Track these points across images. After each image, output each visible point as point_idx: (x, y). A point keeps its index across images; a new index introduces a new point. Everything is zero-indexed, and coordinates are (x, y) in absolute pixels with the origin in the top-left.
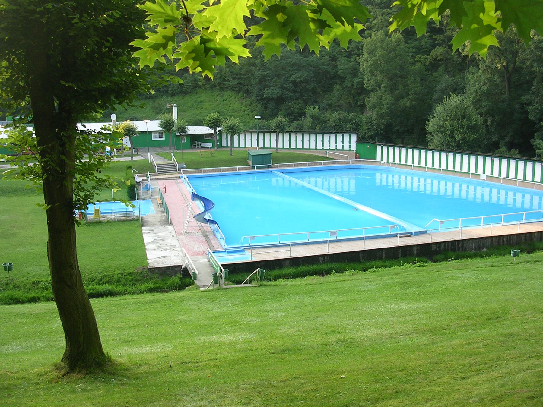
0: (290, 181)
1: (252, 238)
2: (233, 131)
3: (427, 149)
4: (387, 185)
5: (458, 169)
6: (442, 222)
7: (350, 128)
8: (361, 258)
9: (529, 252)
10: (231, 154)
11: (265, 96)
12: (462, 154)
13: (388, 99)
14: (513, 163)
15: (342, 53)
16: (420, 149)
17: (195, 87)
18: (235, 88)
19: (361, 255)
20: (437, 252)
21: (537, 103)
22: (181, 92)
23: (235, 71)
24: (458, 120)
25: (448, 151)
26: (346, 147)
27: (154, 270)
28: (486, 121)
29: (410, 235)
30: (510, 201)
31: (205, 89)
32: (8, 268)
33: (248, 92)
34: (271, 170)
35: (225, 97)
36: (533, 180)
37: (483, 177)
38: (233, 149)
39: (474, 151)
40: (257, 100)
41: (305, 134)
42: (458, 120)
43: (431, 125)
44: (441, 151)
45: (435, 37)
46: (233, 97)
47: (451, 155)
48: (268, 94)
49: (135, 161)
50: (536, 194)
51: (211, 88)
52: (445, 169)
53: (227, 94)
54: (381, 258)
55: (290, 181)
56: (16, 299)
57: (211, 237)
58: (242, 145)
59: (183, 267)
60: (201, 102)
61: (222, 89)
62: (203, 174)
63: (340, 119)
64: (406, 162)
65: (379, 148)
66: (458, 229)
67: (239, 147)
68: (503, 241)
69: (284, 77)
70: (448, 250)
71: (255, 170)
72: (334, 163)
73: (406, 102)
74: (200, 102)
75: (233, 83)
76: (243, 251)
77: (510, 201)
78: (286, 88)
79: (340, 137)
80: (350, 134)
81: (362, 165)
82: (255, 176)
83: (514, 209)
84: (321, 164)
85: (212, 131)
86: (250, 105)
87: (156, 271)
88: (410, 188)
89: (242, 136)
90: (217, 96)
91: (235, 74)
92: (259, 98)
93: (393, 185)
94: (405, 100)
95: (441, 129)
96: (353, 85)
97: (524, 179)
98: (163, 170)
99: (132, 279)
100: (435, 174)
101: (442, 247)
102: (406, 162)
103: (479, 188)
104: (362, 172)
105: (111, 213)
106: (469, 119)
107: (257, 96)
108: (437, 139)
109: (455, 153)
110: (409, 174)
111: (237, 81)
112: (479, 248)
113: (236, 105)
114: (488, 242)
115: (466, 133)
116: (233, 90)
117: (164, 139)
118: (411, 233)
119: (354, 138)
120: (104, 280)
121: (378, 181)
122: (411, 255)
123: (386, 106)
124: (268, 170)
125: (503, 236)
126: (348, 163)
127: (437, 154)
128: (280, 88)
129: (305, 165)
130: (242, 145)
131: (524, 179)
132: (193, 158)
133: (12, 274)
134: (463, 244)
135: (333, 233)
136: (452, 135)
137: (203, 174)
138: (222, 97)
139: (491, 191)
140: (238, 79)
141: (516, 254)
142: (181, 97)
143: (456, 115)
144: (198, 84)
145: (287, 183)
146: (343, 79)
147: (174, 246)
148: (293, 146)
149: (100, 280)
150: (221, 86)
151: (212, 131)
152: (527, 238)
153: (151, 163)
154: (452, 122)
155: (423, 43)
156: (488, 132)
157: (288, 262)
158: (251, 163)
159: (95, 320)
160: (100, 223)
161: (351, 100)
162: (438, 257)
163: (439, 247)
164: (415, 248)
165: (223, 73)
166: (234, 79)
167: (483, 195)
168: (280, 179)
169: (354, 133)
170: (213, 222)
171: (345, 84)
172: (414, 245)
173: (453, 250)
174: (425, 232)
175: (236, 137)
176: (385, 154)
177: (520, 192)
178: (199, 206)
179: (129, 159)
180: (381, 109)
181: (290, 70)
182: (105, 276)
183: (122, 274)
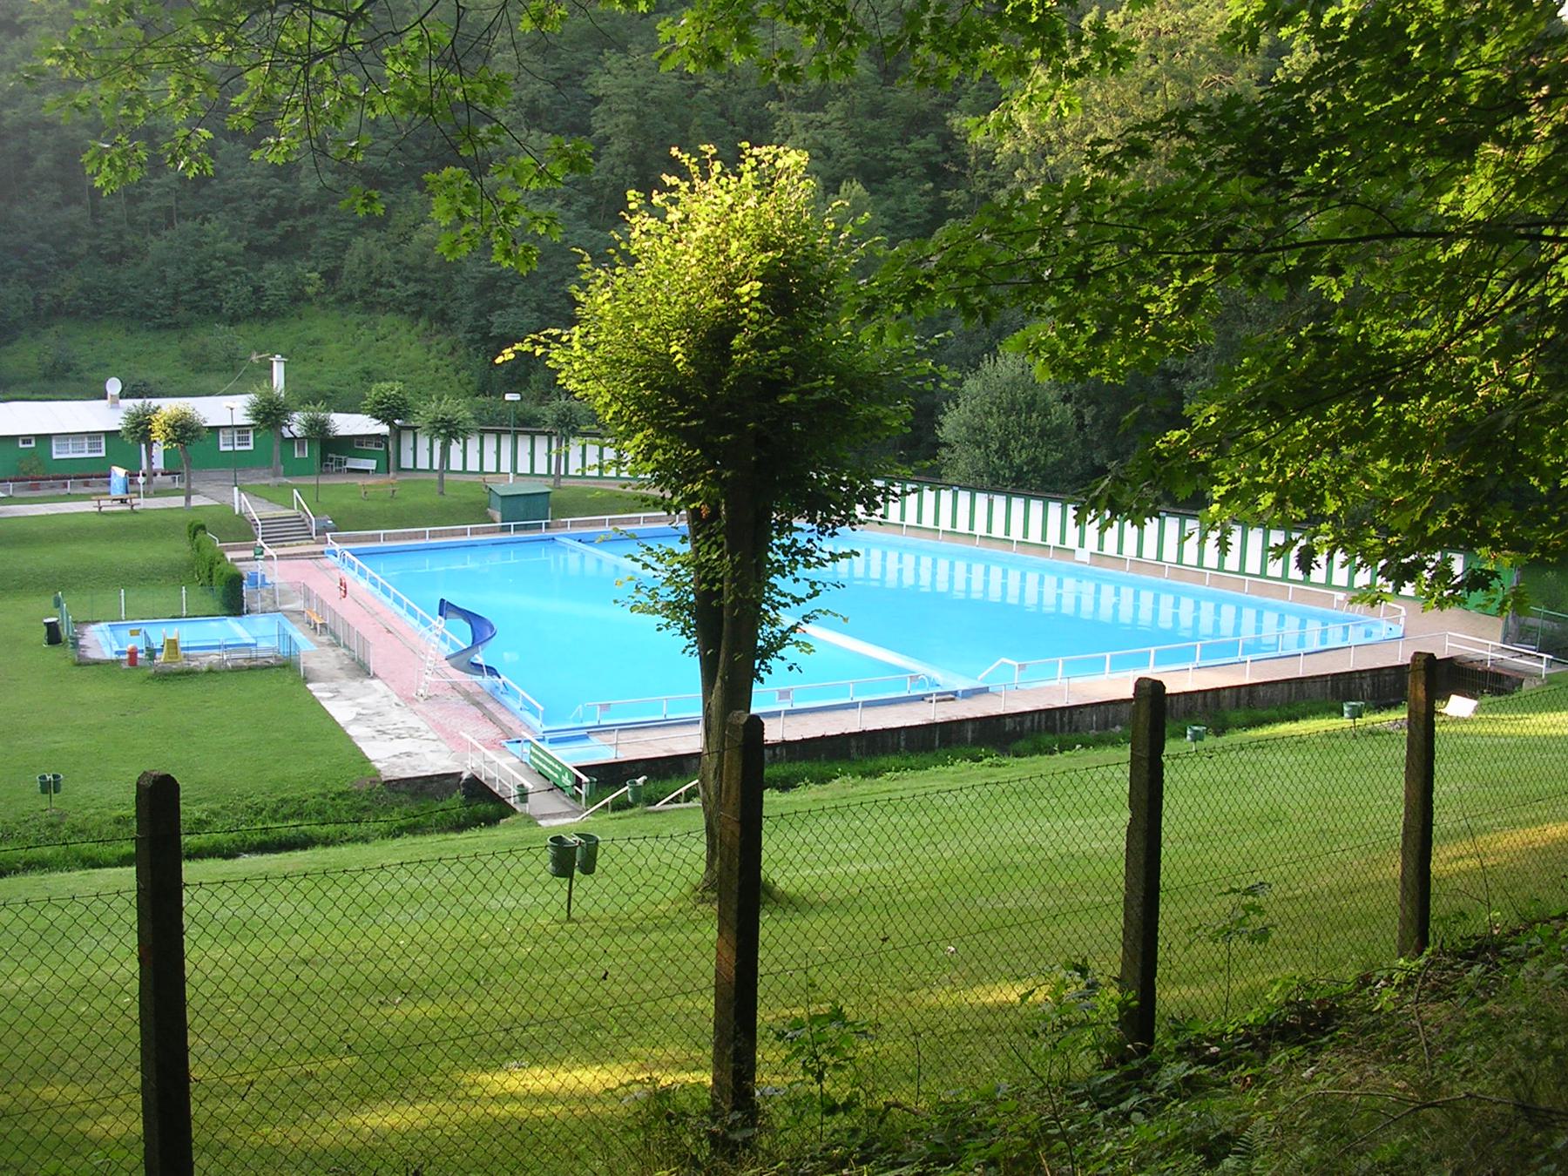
1: (605, 707)
2: (449, 430)
3: (937, 487)
4: (917, 586)
5: (1016, 534)
6: (1022, 667)
8: (853, 751)
9: (1218, 734)
10: (442, 493)
11: (494, 332)
12: (1028, 497)
17: (295, 300)
18: (408, 305)
19: (853, 743)
20: (1017, 735)
21: (1204, 374)
23: (408, 261)
24: (1019, 414)
25: (993, 490)
27: (395, 785)
28: (1079, 415)
29: (952, 696)
30: (1145, 615)
31: (324, 305)
32: (50, 787)
33: (443, 318)
34: (550, 534)
35: (382, 331)
36: (1200, 565)
37: (1083, 555)
38: (446, 477)
39: (1056, 492)
40: (471, 341)
42: (1019, 414)
43: (951, 425)
44: (974, 490)
45: (945, 194)
46: (403, 329)
47: (1000, 501)
48: (504, 325)
50: (1209, 597)
51: (340, 301)
52: (985, 534)
53: (386, 321)
54: (895, 750)
55: (599, 561)
56: (91, 859)
57: (491, 706)
58: (473, 465)
59: (465, 776)
60: (315, 342)
61: (369, 307)
62: (382, 544)
64: (919, 521)
66: (1056, 683)
67: (464, 471)
69: (544, 282)
70: (1039, 731)
71: (512, 535)
74: (313, 343)
75: (404, 290)
76: (586, 737)
77: (1145, 615)
78: (551, 311)
82: (512, 549)
83: (1171, 635)
85: (384, 429)
86: (451, 354)
87: (403, 787)
89: (473, 444)
90: (358, 325)
91: (406, 267)
92: (477, 336)
93: (882, 580)
95: (978, 436)
97: (1179, 562)
98: (280, 532)
99: (351, 808)
100: (961, 546)
101: (1028, 724)
102: (919, 521)
103: (1069, 583)
105: (219, 647)
106: (1045, 413)
107: (472, 330)
108: (964, 460)
109: (1009, 495)
110: (891, 545)
111: (412, 288)
112: (1106, 725)
113: (415, 353)
115: (1037, 446)
116: (402, 311)
117: (251, 447)
118: (955, 693)
120: (286, 810)
122: (962, 741)
124: (544, 533)
127: (964, 496)
128: (533, 310)
130: (473, 465)
131: (1179, 562)
132: (346, 501)
134: (1071, 715)
136: (1003, 451)
137: (382, 544)
138: (373, 328)
139: (1098, 590)
140: (416, 281)
141: (1197, 737)
142: (257, 327)
143: (1013, 403)
144: (302, 292)
147: (418, 730)
149: (275, 811)
150: (370, 298)
151: (384, 429)
152: (1209, 700)
153: (241, 515)
154: (1003, 418)
155: (908, 204)
156: (1085, 442)
158: (498, 516)
160: (190, 673)
162: (1020, 745)
163: (1021, 724)
164: (970, 727)
165: (375, 264)
166: (407, 280)
167: (1078, 600)
168: (573, 559)
172: (968, 720)
173: (1052, 730)
174: (985, 691)
175: (455, 448)
177: (1170, 592)
178: (461, 633)
179: (179, 501)
181: (561, 265)
182: (284, 801)
183: (324, 796)
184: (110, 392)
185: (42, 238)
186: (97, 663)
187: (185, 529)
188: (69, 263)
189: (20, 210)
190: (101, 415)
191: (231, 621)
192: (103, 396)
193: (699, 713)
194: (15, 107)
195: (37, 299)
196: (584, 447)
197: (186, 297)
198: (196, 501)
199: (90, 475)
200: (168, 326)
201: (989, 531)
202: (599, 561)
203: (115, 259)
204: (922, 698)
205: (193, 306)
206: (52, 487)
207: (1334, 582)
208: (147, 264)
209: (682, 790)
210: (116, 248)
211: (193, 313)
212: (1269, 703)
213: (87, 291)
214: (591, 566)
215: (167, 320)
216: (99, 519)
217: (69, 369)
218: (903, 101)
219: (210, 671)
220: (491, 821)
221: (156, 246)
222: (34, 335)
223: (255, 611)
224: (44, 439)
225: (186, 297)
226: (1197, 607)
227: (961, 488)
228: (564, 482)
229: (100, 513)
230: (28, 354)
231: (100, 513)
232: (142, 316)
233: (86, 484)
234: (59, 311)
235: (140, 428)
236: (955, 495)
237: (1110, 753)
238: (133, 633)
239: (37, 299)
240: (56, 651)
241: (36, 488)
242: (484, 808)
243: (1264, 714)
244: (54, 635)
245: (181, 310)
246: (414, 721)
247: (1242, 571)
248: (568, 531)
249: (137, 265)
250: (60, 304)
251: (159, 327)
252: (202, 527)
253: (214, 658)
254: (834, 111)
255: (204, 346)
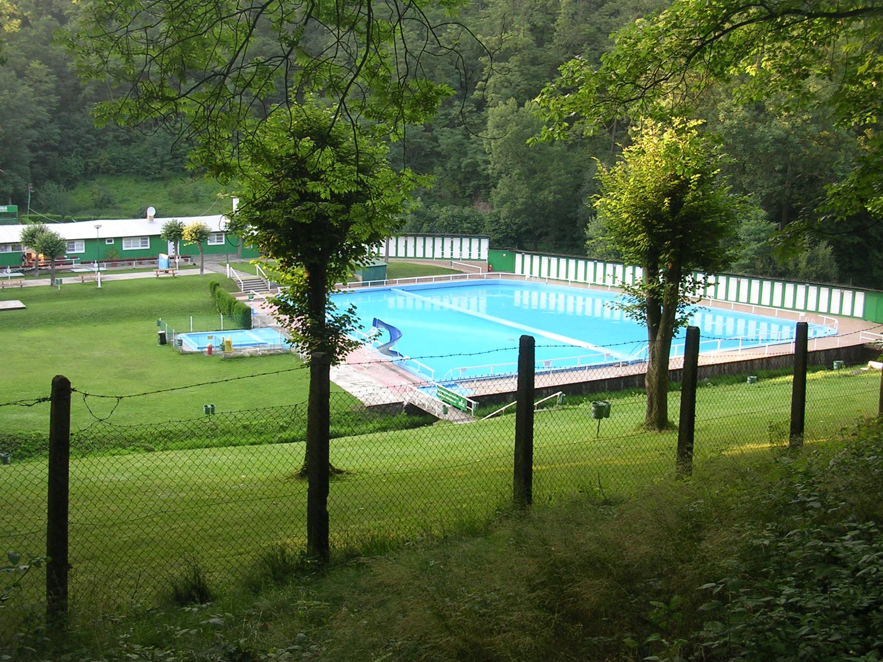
0: (451, 303)
1: (464, 370)
3: (586, 259)
7: (468, 228)
13: (523, 192)
14: (545, 259)
15: (439, 120)
16: (577, 259)
19: (584, 387)
27: (371, 408)
29: (625, 364)
32: (210, 411)
34: (388, 287)
36: (748, 302)
41: (427, 239)
49: (206, 275)
50: (731, 315)
59: (405, 403)
63: (453, 216)
65: (518, 257)
71: (369, 288)
72: (465, 277)
73: (547, 195)
79: (457, 242)
81: (500, 279)
82: (369, 296)
84: (448, 278)
88: (545, 307)
94: (546, 192)
96: (459, 167)
97: (737, 301)
104: (501, 288)
119: (485, 243)
121: (517, 302)
122: (633, 386)
123: (521, 200)
124: (385, 287)
125: (725, 363)
126: (480, 277)
127: (600, 265)
131: (737, 301)
133: (214, 419)
145: (419, 305)
146: (447, 157)
148: (410, 254)
153: (231, 279)
157: (511, 396)
158: (360, 278)
160: (242, 358)
161: (456, 187)
168: (400, 300)
169: (486, 238)
170: (394, 353)
171: (448, 165)
176: (526, 264)
177: (721, 314)
179: (197, 271)
180: (513, 203)
184: (149, 214)
185: (88, 132)
186: (191, 353)
187: (208, 285)
188: (103, 145)
189: (77, 116)
190: (153, 226)
191: (247, 331)
192: (145, 217)
193: (515, 372)
194: (72, 61)
195: (87, 165)
196: (406, 242)
197: (168, 163)
198: (205, 272)
199: (148, 258)
200: (157, 179)
201: (576, 278)
202: (423, 302)
203: (128, 142)
204: (611, 365)
205: (171, 168)
206: (123, 265)
207: (855, 315)
208: (146, 145)
209: (503, 409)
210: (127, 137)
211: (171, 172)
212: (777, 367)
213: (113, 160)
214: (410, 303)
215: (158, 176)
216: (159, 281)
217: (109, 202)
218: (551, 56)
219: (251, 356)
220: (431, 424)
221: (151, 137)
222: (85, 184)
223: (257, 327)
224: (119, 239)
225: (168, 163)
226: (725, 320)
227: (599, 261)
228: (390, 260)
229: (158, 278)
230: (83, 195)
231: (158, 278)
232: (143, 174)
233: (141, 263)
234: (98, 171)
235: (175, 233)
236: (595, 264)
237: (541, 386)
238: (209, 338)
239: (87, 165)
240: (164, 348)
241: (115, 265)
242: (417, 419)
243: (776, 372)
244: (163, 340)
245: (165, 170)
246: (367, 379)
247: (771, 305)
248: (397, 285)
249: (139, 146)
250: (99, 167)
251: (153, 179)
252: (218, 285)
253: (251, 350)
254: (513, 63)
255: (180, 189)
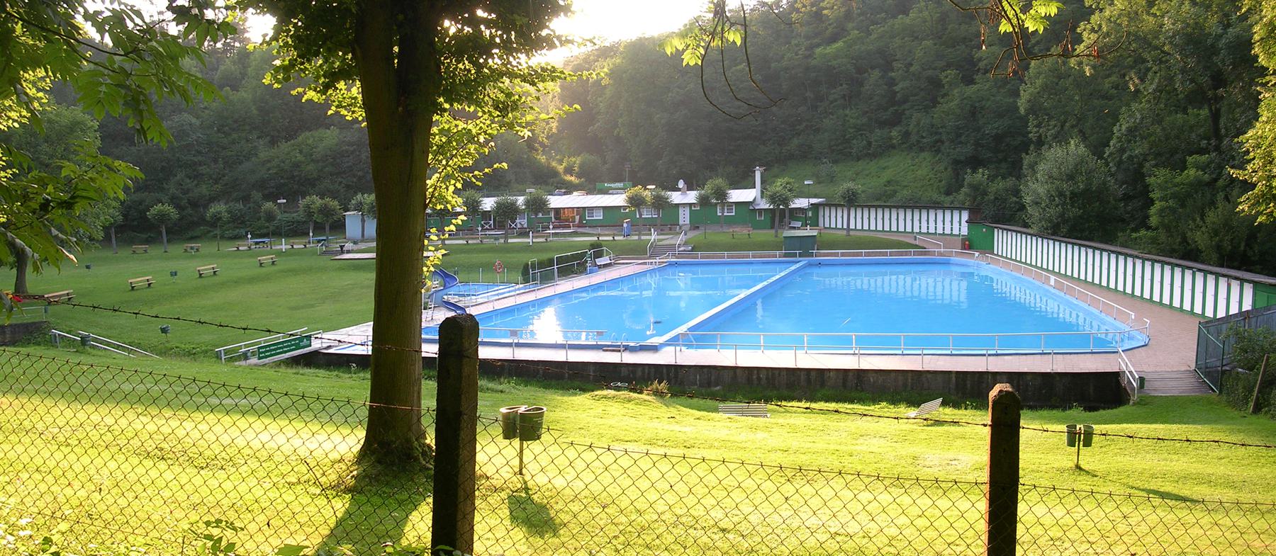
1: (600, 334)
22: (868, 155)
26: (956, 232)
68: (759, 379)
80: (960, 209)
104: (954, 269)
114: (624, 372)
125: (829, 370)
129: (860, 254)
135: (514, 333)
159: (1194, 422)
164: (592, 368)
176: (1008, 243)
